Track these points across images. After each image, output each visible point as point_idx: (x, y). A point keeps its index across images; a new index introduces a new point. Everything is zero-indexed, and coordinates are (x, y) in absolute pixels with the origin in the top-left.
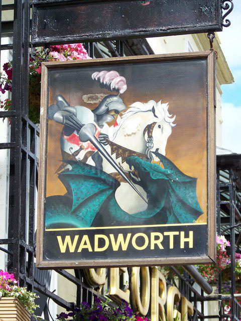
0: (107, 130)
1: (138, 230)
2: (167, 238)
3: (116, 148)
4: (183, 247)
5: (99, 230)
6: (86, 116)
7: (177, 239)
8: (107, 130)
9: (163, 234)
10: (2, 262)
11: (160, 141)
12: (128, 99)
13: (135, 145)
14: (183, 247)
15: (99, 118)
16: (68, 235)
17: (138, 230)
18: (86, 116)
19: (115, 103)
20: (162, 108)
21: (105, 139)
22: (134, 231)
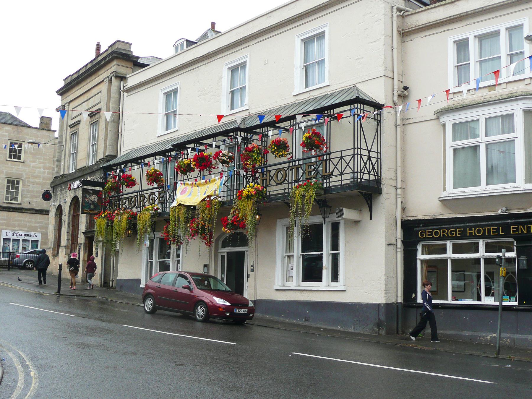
0: (90, 198)
1: (451, 228)
2: (484, 230)
3: (91, 200)
4: (433, 302)
5: (497, 221)
6: (88, 196)
7: (489, 230)
8: (90, 198)
9: (433, 236)
10: (18, 108)
11: (96, 200)
12: (93, 194)
13: (93, 200)
14: (433, 302)
15: (89, 196)
16: (504, 248)
17: (451, 228)
18: (88, 196)
19: (91, 195)
20: (96, 196)
21: (90, 199)
22: (475, 227)
